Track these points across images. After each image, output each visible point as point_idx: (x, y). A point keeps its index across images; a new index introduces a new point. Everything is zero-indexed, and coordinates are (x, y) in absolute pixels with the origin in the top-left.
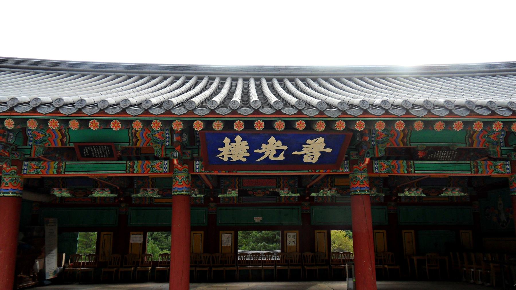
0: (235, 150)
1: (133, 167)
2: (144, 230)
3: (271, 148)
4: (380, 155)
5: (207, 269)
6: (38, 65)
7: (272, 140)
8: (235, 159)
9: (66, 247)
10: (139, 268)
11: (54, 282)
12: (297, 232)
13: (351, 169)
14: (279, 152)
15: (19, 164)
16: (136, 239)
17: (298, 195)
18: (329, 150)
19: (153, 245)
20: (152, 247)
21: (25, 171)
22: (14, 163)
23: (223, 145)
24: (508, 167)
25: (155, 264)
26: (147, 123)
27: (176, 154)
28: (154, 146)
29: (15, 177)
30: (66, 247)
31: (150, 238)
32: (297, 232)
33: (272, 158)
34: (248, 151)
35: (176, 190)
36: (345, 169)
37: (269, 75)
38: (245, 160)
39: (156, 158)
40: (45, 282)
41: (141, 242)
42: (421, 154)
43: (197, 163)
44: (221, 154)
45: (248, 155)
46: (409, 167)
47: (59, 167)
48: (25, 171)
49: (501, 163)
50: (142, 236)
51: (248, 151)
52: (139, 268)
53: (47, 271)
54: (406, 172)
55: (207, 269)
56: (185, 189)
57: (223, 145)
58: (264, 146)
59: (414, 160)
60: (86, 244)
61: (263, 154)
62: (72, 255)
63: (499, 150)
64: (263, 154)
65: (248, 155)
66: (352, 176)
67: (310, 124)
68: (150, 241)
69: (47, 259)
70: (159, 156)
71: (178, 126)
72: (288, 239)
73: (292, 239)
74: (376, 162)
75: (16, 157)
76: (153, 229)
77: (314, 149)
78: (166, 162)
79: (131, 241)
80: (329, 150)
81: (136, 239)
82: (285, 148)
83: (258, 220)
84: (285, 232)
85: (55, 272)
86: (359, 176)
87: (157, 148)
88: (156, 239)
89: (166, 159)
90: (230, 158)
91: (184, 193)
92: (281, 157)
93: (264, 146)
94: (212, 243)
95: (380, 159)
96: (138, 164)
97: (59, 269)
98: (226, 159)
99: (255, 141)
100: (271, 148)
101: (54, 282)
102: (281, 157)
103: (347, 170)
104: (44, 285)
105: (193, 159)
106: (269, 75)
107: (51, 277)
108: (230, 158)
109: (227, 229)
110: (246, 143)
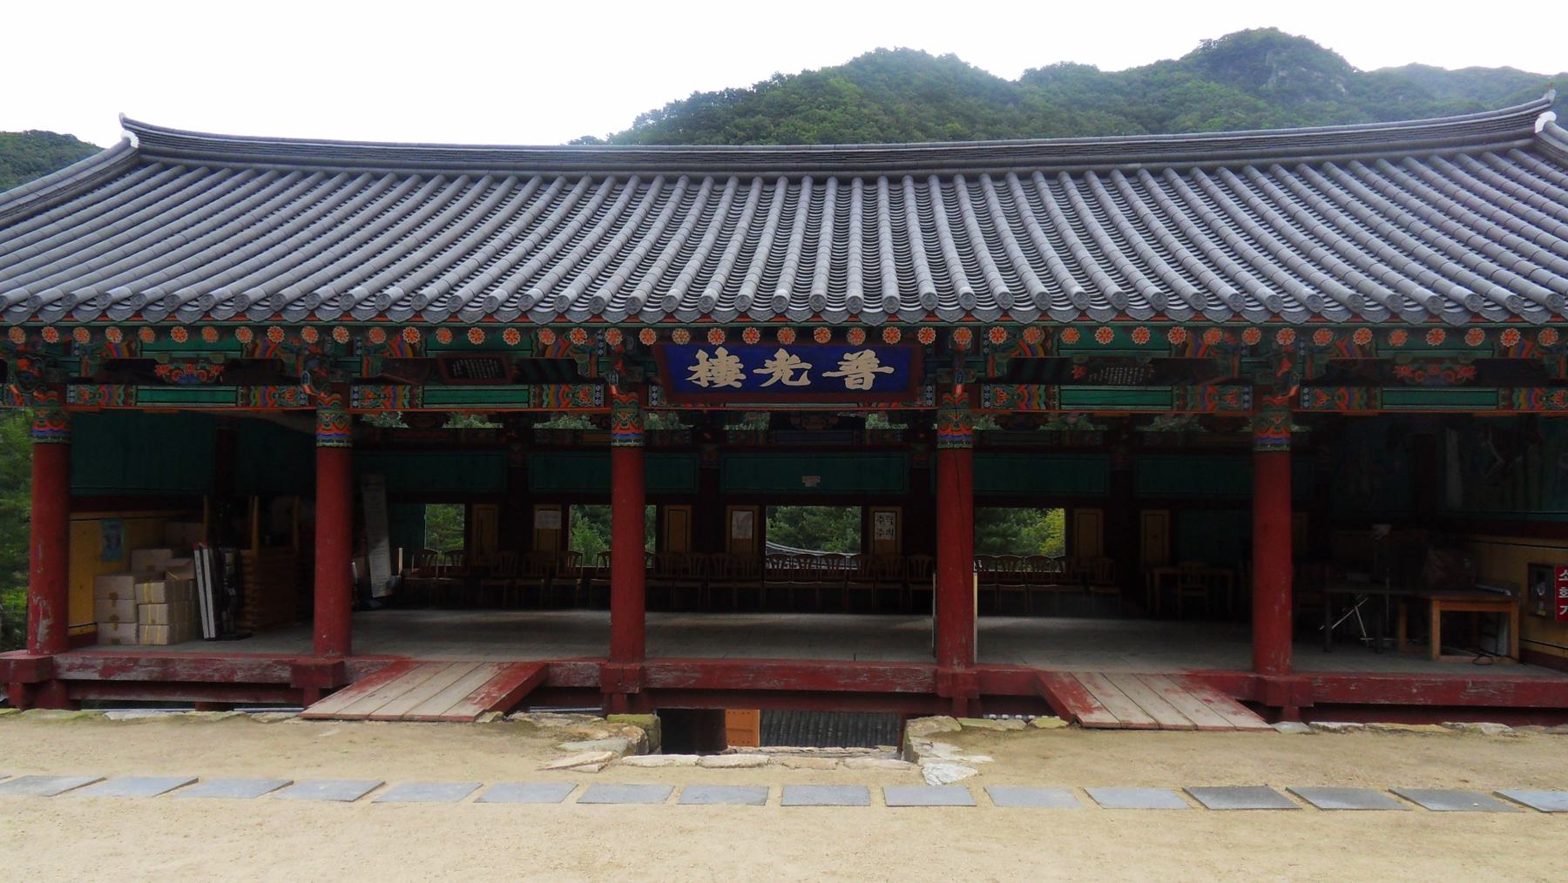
0: (719, 369)
1: (540, 395)
2: (563, 500)
3: (782, 366)
4: (997, 374)
5: (698, 585)
6: (329, 155)
7: (781, 354)
8: (721, 383)
9: (406, 535)
10: (555, 581)
11: (388, 603)
12: (899, 509)
13: (938, 401)
14: (797, 374)
15: (343, 390)
16: (545, 519)
17: (904, 426)
18: (889, 370)
19: (588, 533)
20: (585, 539)
21: (355, 403)
22: (335, 388)
23: (697, 362)
24: (1246, 397)
25: (590, 573)
26: (561, 332)
27: (614, 378)
28: (576, 358)
29: (340, 413)
30: (406, 535)
31: (579, 515)
32: (899, 509)
33: (786, 381)
34: (742, 371)
35: (617, 438)
36: (926, 401)
37: (821, 169)
38: (739, 385)
39: (581, 380)
40: (373, 604)
41: (558, 526)
42: (1077, 372)
43: (654, 388)
44: (695, 377)
45: (743, 377)
46: (1050, 397)
47: (413, 397)
48: (355, 403)
49: (1235, 389)
50: (559, 514)
51: (742, 371)
52: (555, 581)
53: (373, 581)
54: (1043, 407)
55: (698, 585)
56: (632, 437)
57: (697, 362)
58: (768, 363)
59: (1060, 383)
60: (444, 524)
61: (770, 376)
62: (415, 550)
63: (1237, 364)
64: (770, 376)
65: (743, 377)
66: (940, 413)
67: (839, 332)
68: (579, 523)
69: (371, 558)
70: (587, 375)
71: (614, 339)
72: (878, 526)
73: (886, 525)
74: (987, 388)
75: (338, 378)
76: (582, 499)
77: (860, 369)
78: (598, 388)
79: (537, 525)
80: (889, 370)
81: (545, 519)
82: (809, 366)
83: (810, 482)
84: (872, 509)
85: (388, 583)
86: (952, 414)
87: (581, 360)
88: (594, 518)
89: (600, 381)
90: (711, 383)
91: (632, 444)
92: (804, 381)
93: (768, 363)
94: (709, 530)
95: (997, 381)
96: (257, 393)
97: (394, 580)
98: (704, 384)
99: (752, 358)
100: (782, 366)
101: (388, 603)
102: (804, 381)
103: (930, 402)
104: (367, 608)
105: (648, 382)
106: (821, 169)
107: (382, 593)
108: (711, 383)
109: (743, 500)
110: (735, 358)
